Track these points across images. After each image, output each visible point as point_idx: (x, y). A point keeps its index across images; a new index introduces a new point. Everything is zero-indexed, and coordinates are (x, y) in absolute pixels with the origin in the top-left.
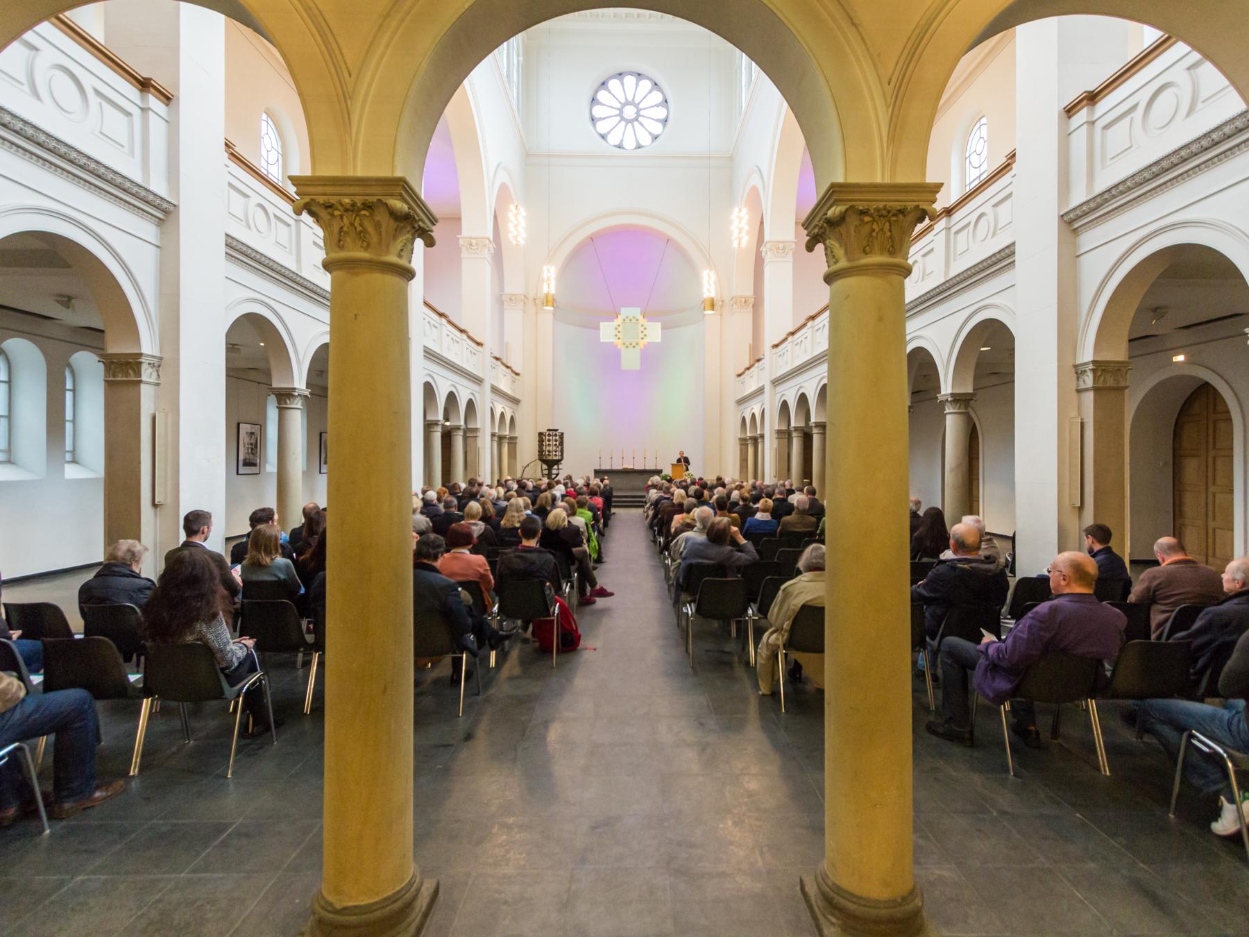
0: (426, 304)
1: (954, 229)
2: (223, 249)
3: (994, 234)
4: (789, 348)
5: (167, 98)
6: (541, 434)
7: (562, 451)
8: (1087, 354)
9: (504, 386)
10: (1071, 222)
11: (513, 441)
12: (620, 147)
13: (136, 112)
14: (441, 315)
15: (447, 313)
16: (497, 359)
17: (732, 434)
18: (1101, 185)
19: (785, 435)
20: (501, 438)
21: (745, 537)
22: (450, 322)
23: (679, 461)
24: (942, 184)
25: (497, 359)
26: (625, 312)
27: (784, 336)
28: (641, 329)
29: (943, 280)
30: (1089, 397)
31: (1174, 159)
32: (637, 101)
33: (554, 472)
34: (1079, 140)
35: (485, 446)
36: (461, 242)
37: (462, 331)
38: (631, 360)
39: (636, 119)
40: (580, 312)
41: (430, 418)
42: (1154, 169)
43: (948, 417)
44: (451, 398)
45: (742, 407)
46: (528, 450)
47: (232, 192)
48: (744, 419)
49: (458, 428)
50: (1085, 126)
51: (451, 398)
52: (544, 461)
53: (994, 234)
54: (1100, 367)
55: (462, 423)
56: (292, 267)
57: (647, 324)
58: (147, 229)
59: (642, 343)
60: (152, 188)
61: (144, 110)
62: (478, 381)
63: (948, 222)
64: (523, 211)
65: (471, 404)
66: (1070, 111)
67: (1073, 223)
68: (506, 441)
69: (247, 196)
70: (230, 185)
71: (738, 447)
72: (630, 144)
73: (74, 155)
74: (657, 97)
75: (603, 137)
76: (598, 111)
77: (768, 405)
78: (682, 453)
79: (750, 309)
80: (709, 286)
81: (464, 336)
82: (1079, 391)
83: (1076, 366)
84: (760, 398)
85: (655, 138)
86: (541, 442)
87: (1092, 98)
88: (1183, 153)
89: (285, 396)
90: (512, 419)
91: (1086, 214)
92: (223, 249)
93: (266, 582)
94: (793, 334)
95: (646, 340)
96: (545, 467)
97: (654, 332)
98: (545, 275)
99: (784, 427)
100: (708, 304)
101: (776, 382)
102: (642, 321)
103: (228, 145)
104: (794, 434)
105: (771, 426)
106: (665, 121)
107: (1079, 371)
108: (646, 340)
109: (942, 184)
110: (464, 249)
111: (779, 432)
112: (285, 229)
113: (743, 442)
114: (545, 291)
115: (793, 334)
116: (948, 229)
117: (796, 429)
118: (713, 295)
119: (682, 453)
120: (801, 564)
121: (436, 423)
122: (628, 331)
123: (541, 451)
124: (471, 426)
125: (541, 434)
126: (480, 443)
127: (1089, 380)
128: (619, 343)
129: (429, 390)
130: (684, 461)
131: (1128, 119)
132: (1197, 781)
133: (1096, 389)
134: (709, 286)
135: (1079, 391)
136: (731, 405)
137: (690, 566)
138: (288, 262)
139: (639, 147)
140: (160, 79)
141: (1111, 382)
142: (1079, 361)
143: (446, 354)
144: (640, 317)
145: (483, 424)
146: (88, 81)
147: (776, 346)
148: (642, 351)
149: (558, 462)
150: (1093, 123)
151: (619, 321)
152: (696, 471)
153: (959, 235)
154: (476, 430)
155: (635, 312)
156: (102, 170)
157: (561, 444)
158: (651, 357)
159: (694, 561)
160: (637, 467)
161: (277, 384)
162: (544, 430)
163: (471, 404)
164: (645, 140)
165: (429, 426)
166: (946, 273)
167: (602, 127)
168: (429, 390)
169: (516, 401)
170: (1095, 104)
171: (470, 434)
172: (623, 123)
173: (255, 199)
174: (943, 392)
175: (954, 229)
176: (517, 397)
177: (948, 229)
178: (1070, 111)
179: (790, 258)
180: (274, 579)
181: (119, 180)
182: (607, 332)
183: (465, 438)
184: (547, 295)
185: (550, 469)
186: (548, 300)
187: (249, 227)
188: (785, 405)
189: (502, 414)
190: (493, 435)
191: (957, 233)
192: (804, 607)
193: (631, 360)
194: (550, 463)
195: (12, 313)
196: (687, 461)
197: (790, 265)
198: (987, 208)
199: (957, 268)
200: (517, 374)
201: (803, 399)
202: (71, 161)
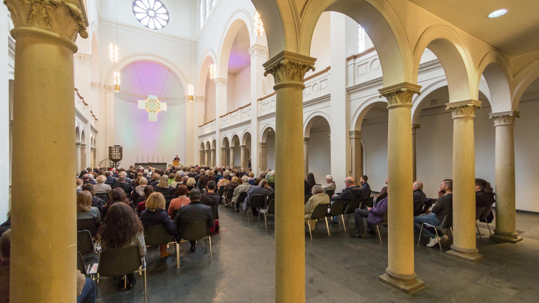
1: (357, 65)
4: (229, 118)
6: (110, 148)
7: (121, 155)
8: (353, 129)
12: (147, 26)
17: (197, 149)
18: (358, 82)
19: (226, 150)
23: (175, 159)
24: (479, 91)
26: (150, 97)
30: (353, 141)
32: (155, 9)
34: (351, 68)
38: (153, 117)
39: (155, 17)
40: (129, 95)
46: (103, 154)
48: (203, 144)
52: (112, 160)
54: (357, 132)
57: (160, 103)
59: (158, 111)
62: (86, 121)
64: (117, 48)
66: (258, 100)
67: (349, 91)
71: (199, 154)
72: (152, 26)
74: (163, 10)
75: (139, 21)
76: (136, 9)
78: (177, 156)
79: (204, 102)
80: (190, 91)
82: (350, 139)
83: (350, 132)
85: (163, 27)
87: (355, 57)
91: (353, 89)
93: (87, 219)
95: (160, 110)
97: (164, 107)
98: (115, 76)
100: (190, 98)
101: (221, 130)
104: (242, 148)
105: (219, 146)
106: (168, 21)
107: (350, 133)
109: (479, 91)
110: (76, 58)
111: (223, 148)
113: (203, 153)
114: (115, 83)
117: (232, 147)
118: (192, 94)
119: (177, 156)
120: (312, 192)
122: (152, 105)
125: (110, 148)
127: (353, 136)
128: (148, 110)
130: (177, 159)
131: (365, 65)
132: (425, 235)
133: (356, 139)
134: (190, 91)
135: (350, 139)
136: (196, 138)
137: (253, 197)
139: (156, 29)
141: (358, 137)
142: (351, 130)
147: (221, 117)
152: (182, 163)
155: (155, 97)
158: (162, 116)
159: (255, 195)
162: (112, 146)
164: (159, 27)
167: (139, 16)
169: (96, 132)
172: (148, 17)
178: (348, 59)
179: (226, 85)
180: (92, 217)
182: (142, 104)
184: (116, 86)
185: (116, 163)
186: (116, 87)
188: (226, 140)
190: (92, 149)
192: (319, 205)
197: (226, 88)
198: (318, 82)
201: (236, 137)
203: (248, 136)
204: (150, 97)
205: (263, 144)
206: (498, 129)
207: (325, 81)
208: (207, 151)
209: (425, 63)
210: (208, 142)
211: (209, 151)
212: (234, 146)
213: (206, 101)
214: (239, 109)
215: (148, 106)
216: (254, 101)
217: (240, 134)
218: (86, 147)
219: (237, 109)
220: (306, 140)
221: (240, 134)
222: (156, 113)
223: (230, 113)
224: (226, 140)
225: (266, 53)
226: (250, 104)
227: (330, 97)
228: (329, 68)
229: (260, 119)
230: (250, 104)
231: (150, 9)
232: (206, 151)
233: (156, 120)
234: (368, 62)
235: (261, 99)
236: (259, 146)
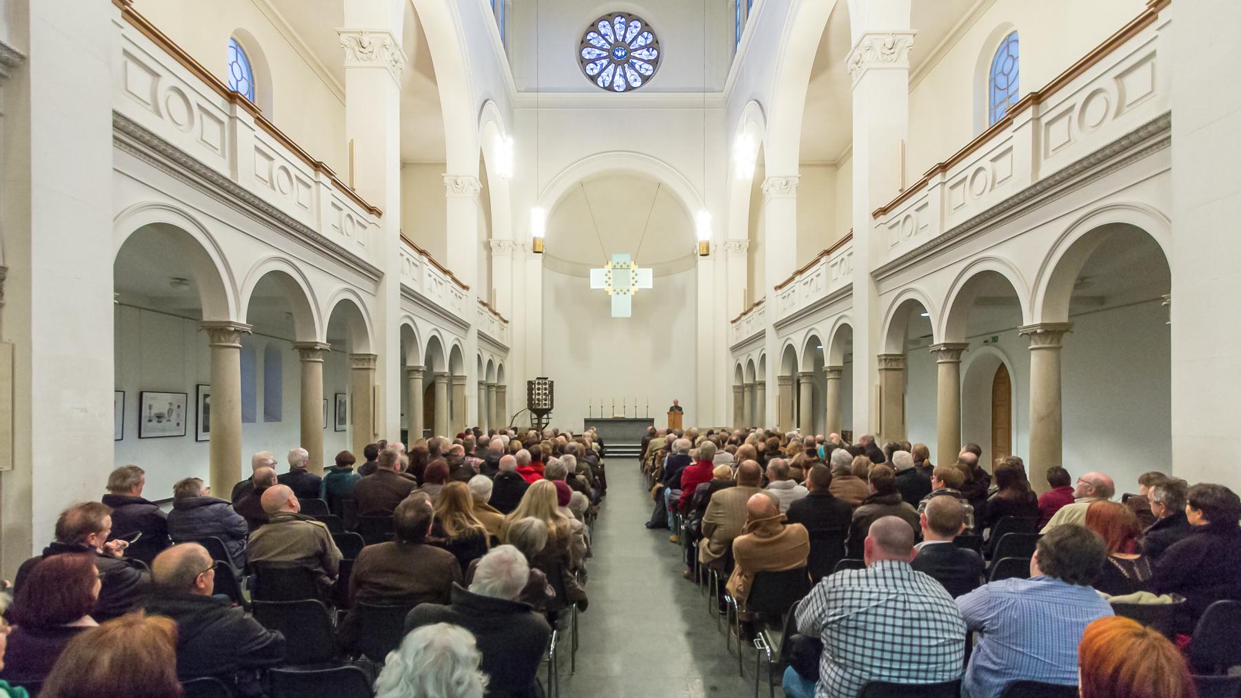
0: (403, 238)
1: (1044, 120)
2: (399, 291)
3: (1117, 114)
5: (379, 214)
6: (530, 383)
9: (493, 331)
10: (876, 276)
11: (501, 390)
13: (225, 119)
14: (421, 252)
15: (428, 251)
16: (484, 304)
19: (792, 382)
20: (489, 386)
22: (431, 261)
23: (672, 409)
25: (484, 304)
27: (815, 257)
28: (633, 275)
29: (1029, 184)
33: (544, 421)
35: (471, 392)
36: (446, 180)
37: (446, 272)
38: (622, 307)
41: (410, 363)
42: (1123, 143)
44: (434, 343)
45: (737, 353)
46: (516, 398)
47: (258, 156)
48: (739, 365)
49: (442, 375)
50: (1030, 124)
51: (434, 343)
53: (1117, 114)
55: (447, 370)
56: (226, 173)
57: (638, 270)
58: (369, 285)
59: (633, 290)
60: (240, 183)
61: (233, 118)
62: (464, 326)
63: (1036, 112)
65: (456, 350)
66: (875, 215)
68: (493, 391)
69: (272, 159)
70: (257, 149)
71: (732, 396)
73: (197, 167)
77: (773, 347)
78: (676, 402)
81: (448, 278)
84: (759, 343)
86: (530, 390)
88: (1123, 143)
89: (307, 350)
90: (501, 366)
92: (109, 131)
94: (801, 272)
95: (636, 288)
96: (534, 416)
99: (738, 384)
101: (779, 326)
102: (633, 267)
103: (379, 214)
104: (830, 376)
105: (774, 371)
112: (217, 127)
113: (740, 390)
115: (801, 272)
116: (1036, 119)
119: (676, 402)
121: (417, 370)
123: (530, 400)
124: (457, 374)
125: (530, 383)
126: (376, 379)
128: (610, 290)
129: (407, 334)
138: (220, 166)
140: (379, 207)
143: (245, 181)
145: (470, 371)
146: (193, 98)
147: (780, 287)
148: (640, 266)
149: (547, 411)
150: (1038, 119)
151: (609, 267)
153: (1053, 128)
154: (463, 378)
155: (624, 258)
156: (155, 142)
157: (551, 392)
160: (628, 416)
161: (207, 316)
162: (533, 379)
163: (456, 350)
165: (407, 373)
166: (942, 227)
168: (407, 334)
170: (1039, 103)
171: (455, 381)
173: (279, 162)
175: (1044, 120)
176: (506, 344)
177: (1036, 119)
178: (875, 215)
179: (793, 194)
181: (147, 137)
183: (450, 387)
187: (159, 115)
188: (790, 350)
189: (490, 361)
190: (480, 383)
191: (952, 188)
193: (622, 307)
194: (540, 412)
196: (680, 409)
198: (1107, 82)
199: (1049, 168)
200: (506, 322)
201: (814, 341)
202: (128, 133)
203: (844, 335)
204: (619, 258)
205: (887, 358)
206: (829, 382)
207: (1008, 156)
208: (748, 391)
210: (751, 362)
211: (817, 377)
212: (810, 369)
214: (931, 174)
215: (610, 282)
216: (860, 220)
217: (825, 329)
218: (467, 382)
219: (920, 177)
220: (1052, 332)
223: (828, 252)
224: (790, 350)
225: (905, 53)
226: (850, 237)
227: (1168, 127)
228: (1169, 22)
230: (850, 237)
231: (628, 52)
232: (833, 369)
235: (884, 211)
236: (877, 366)
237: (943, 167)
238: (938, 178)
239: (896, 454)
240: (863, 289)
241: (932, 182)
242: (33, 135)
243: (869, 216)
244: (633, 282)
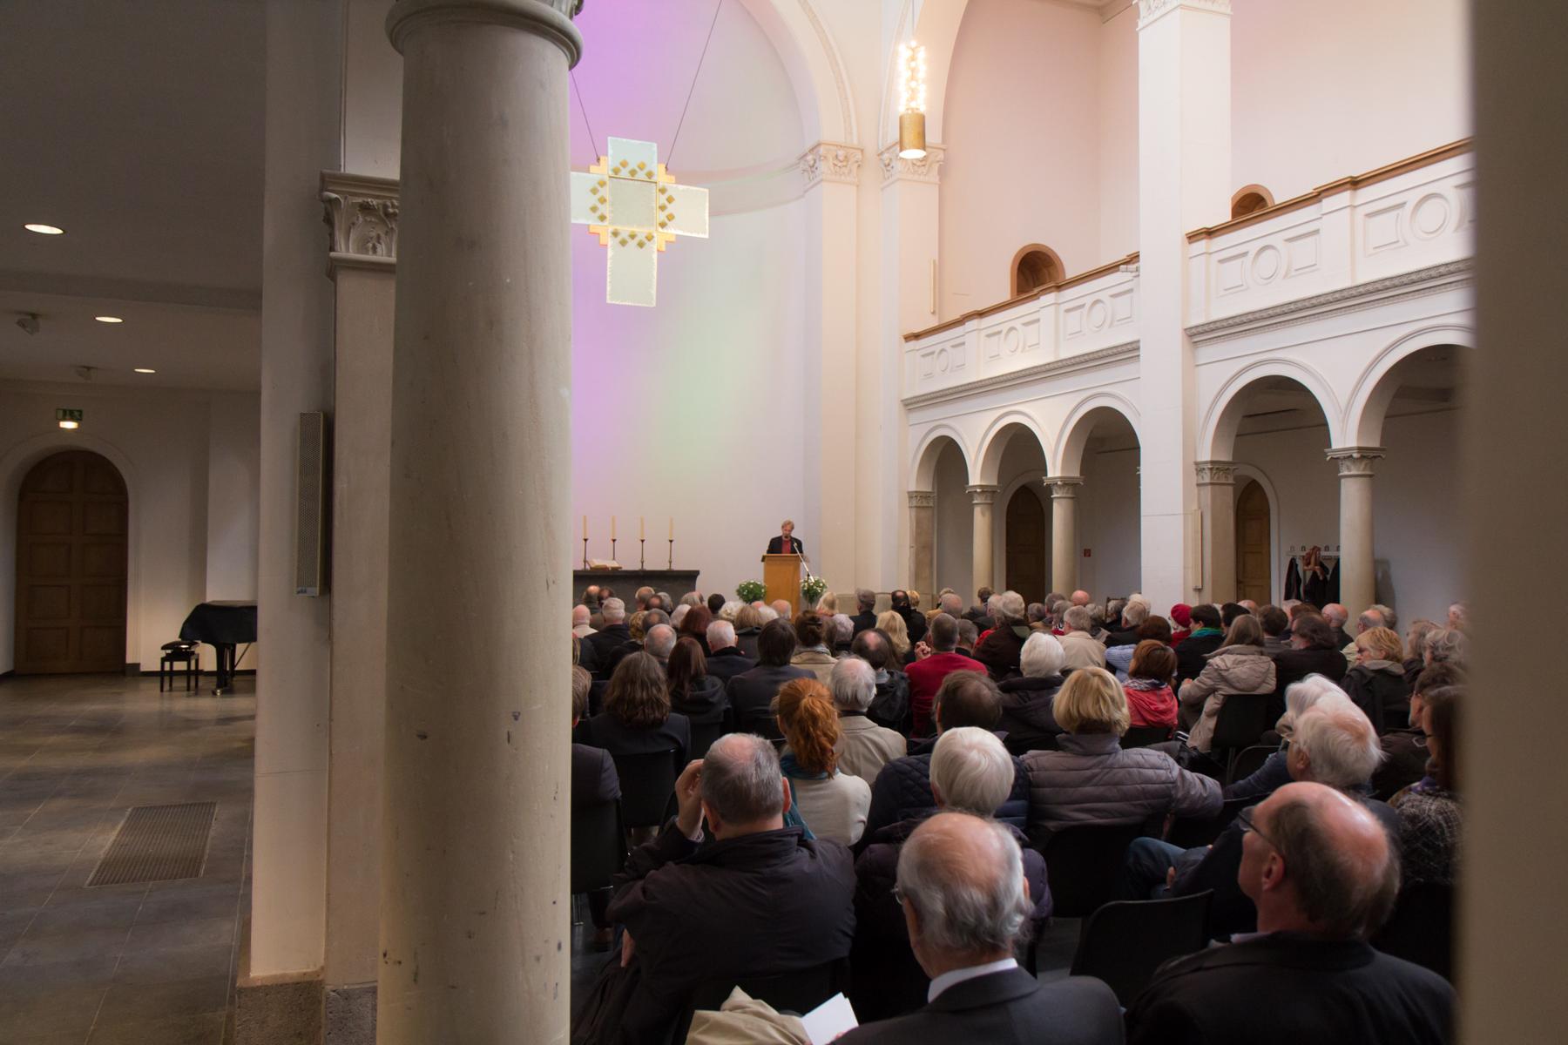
17: (896, 471)
21: (690, 614)
23: (776, 546)
31: (1433, 273)
43: (1055, 505)
53: (1111, 325)
59: (662, 237)
64: (922, 54)
66: (1193, 237)
78: (788, 526)
79: (934, 176)
83: (1197, 464)
95: (672, 231)
97: (692, 212)
100: (910, 136)
102: (662, 178)
108: (672, 231)
118: (923, 109)
119: (788, 526)
130: (783, 547)
142: (1200, 459)
144: (659, 170)
148: (678, 182)
155: (643, 152)
174: (1050, 474)
178: (1193, 237)
195: (340, 485)
201: (1017, 445)
209: (1295, 302)
213: (943, 172)
215: (605, 209)
217: (1052, 422)
219: (956, 316)
221: (1052, 422)
222: (654, 246)
229: (1199, 335)
233: (648, 296)
234: (1402, 205)
235: (917, 336)
236: (1194, 479)
237: (1355, 183)
238: (1345, 197)
239: (992, 599)
240: (1164, 353)
241: (1329, 203)
242: (392, 348)
243: (1180, 238)
244: (662, 216)
